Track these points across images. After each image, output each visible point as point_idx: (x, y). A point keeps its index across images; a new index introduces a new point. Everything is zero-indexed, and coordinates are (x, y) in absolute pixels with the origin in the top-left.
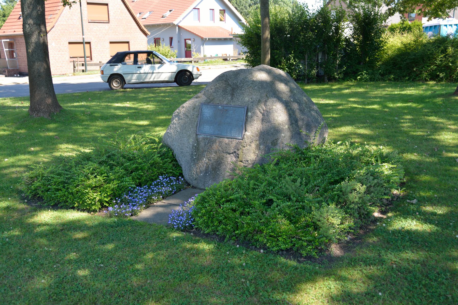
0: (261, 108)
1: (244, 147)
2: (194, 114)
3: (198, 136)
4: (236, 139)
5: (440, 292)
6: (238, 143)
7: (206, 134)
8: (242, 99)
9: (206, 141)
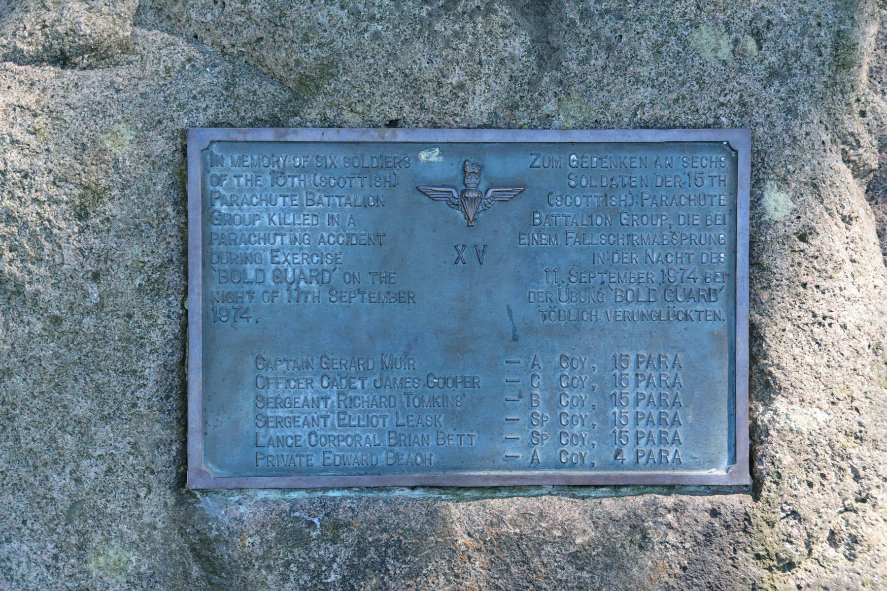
0: (855, 125)
1: (789, 566)
2: (105, 257)
3: (207, 504)
4: (670, 488)
5: (804, 407)
6: (709, 536)
7: (309, 471)
8: (657, 50)
9: (325, 551)
